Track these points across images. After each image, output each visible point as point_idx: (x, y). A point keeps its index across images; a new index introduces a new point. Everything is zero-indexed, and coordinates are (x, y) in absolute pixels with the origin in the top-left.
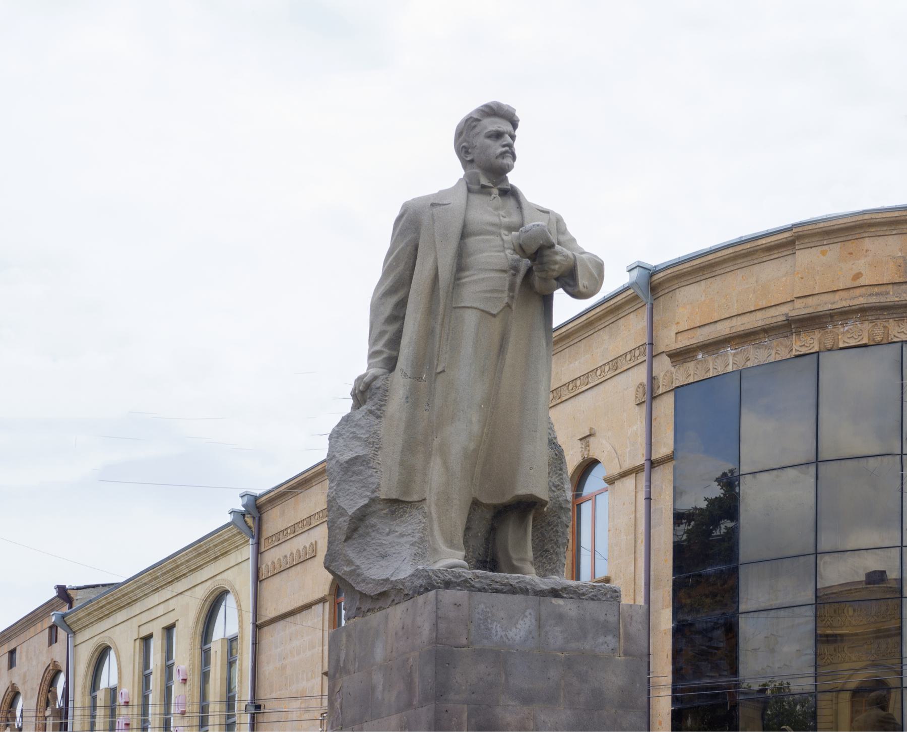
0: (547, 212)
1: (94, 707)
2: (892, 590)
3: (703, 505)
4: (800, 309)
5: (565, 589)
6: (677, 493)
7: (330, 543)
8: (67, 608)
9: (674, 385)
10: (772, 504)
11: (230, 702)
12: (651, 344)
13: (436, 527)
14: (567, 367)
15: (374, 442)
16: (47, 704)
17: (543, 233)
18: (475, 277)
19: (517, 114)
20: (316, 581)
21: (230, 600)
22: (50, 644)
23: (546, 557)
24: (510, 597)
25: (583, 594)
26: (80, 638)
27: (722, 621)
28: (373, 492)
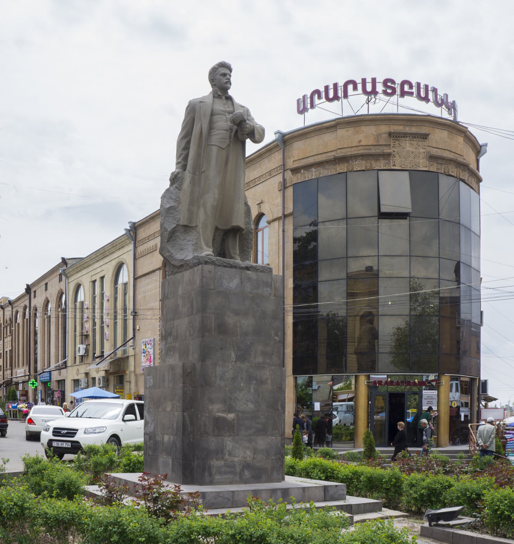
0: (243, 107)
1: (75, 308)
2: (375, 275)
3: (304, 235)
4: (339, 154)
5: (252, 267)
6: (295, 229)
7: (161, 243)
8: (66, 268)
9: (293, 183)
10: (331, 235)
11: (125, 310)
12: (284, 165)
13: (202, 240)
14: (251, 174)
15: (178, 200)
16: (59, 307)
17: (241, 115)
18: (216, 133)
19: (232, 67)
20: (157, 260)
21: (125, 266)
22: (60, 282)
23: (244, 253)
24: (230, 269)
25: (258, 269)
26: (71, 279)
27: (311, 285)
28: (178, 221)
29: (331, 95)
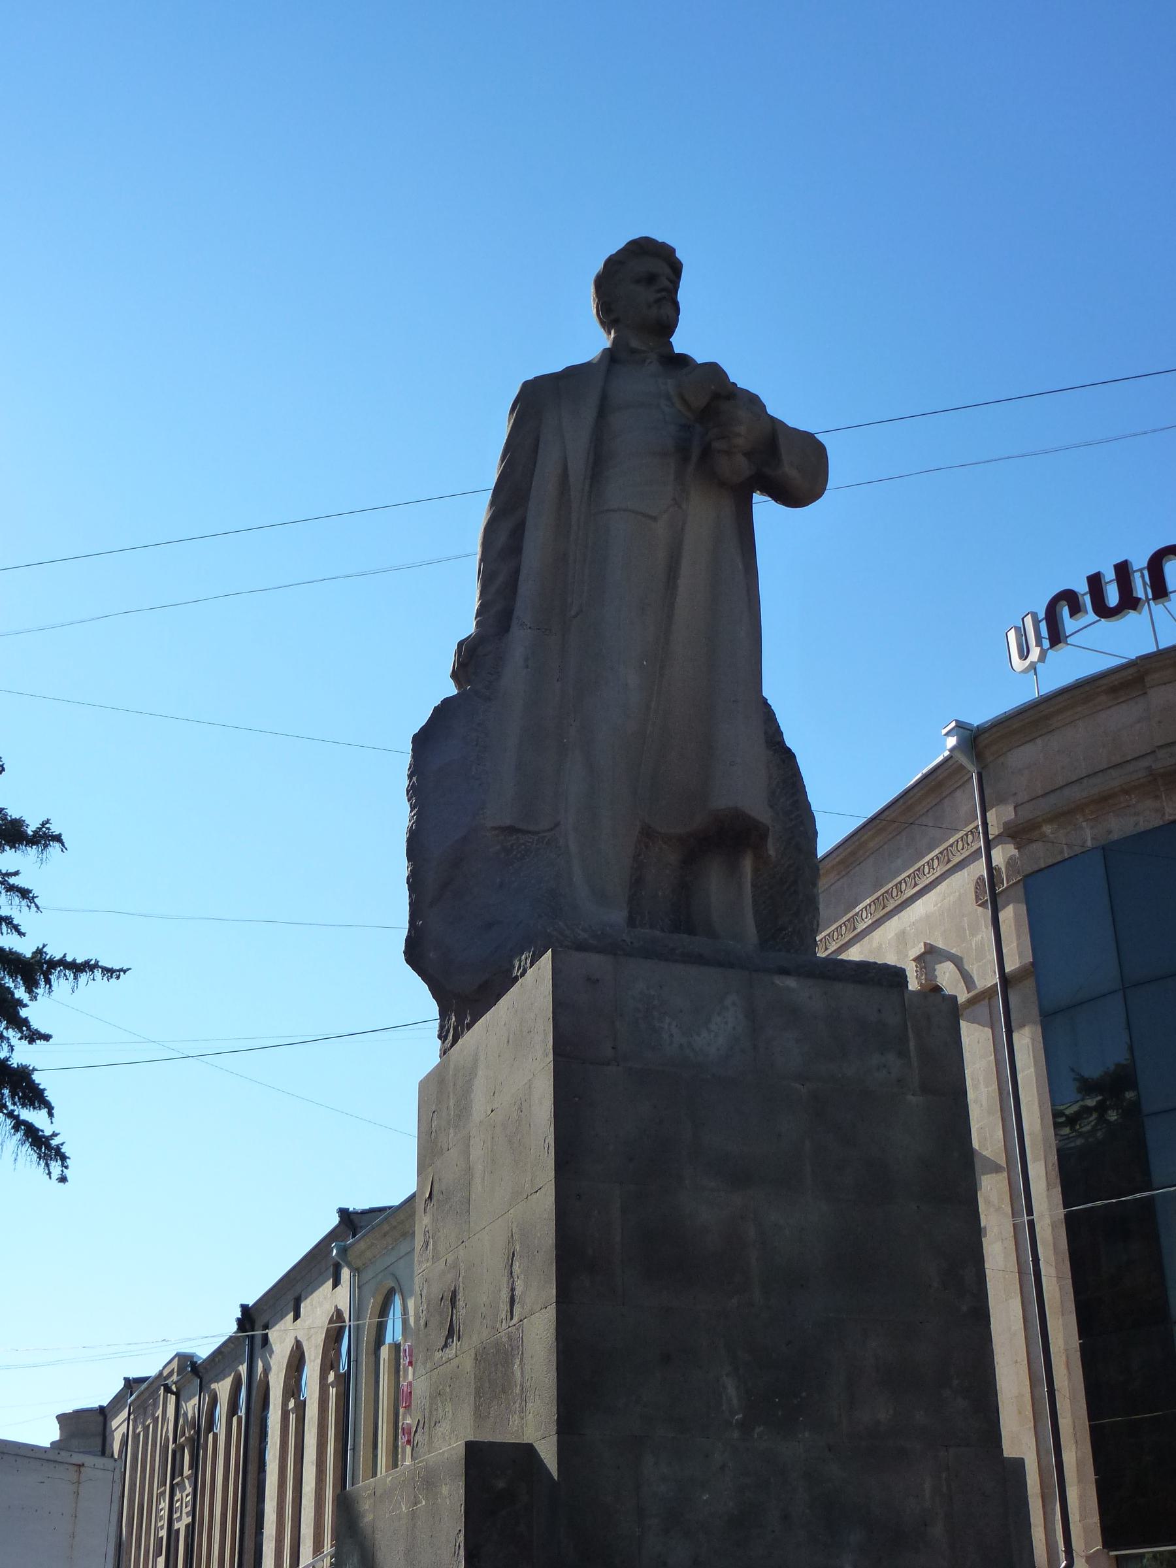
19: (679, 255)
29: (1113, 597)
